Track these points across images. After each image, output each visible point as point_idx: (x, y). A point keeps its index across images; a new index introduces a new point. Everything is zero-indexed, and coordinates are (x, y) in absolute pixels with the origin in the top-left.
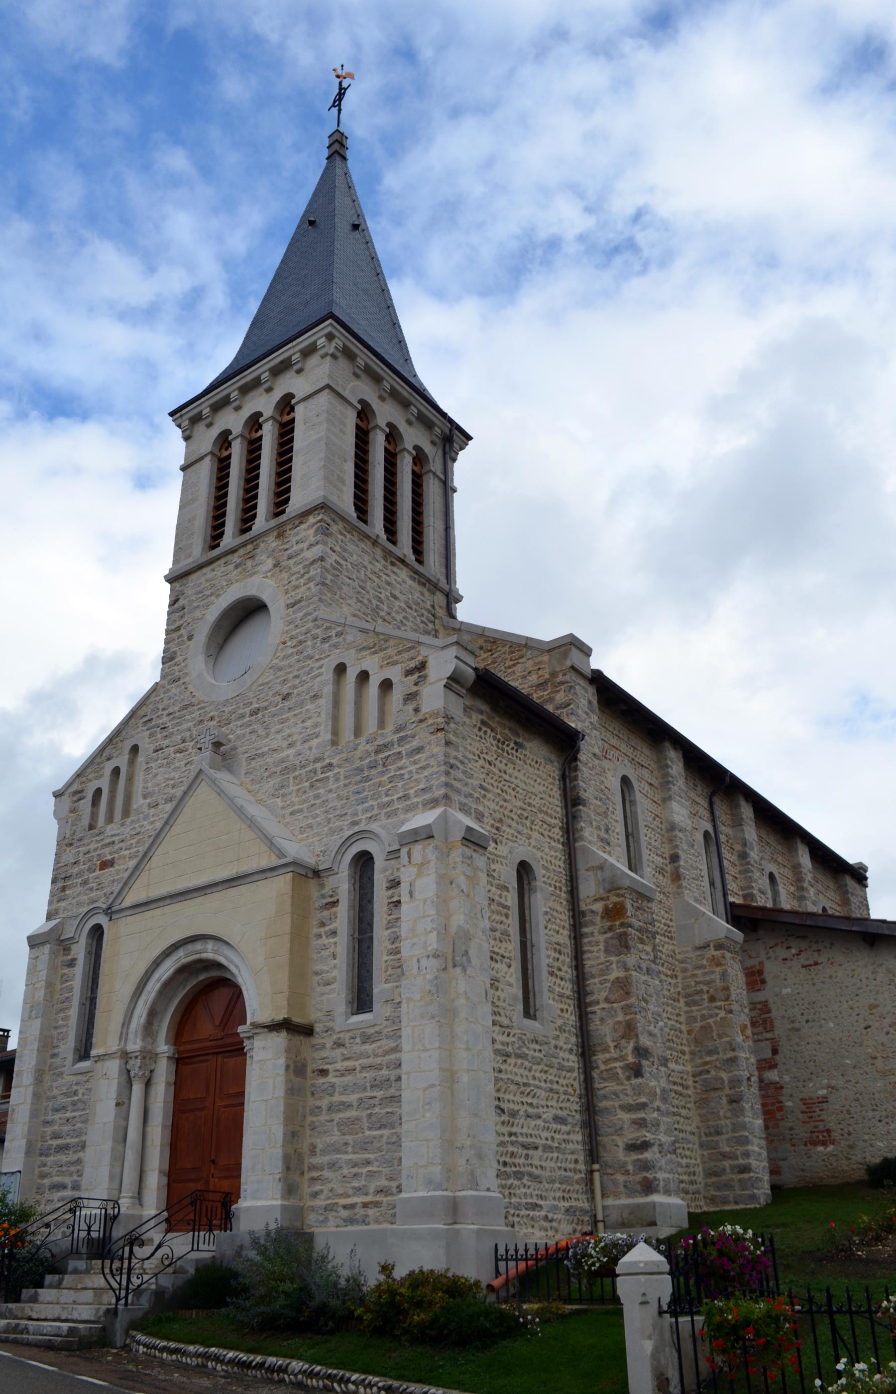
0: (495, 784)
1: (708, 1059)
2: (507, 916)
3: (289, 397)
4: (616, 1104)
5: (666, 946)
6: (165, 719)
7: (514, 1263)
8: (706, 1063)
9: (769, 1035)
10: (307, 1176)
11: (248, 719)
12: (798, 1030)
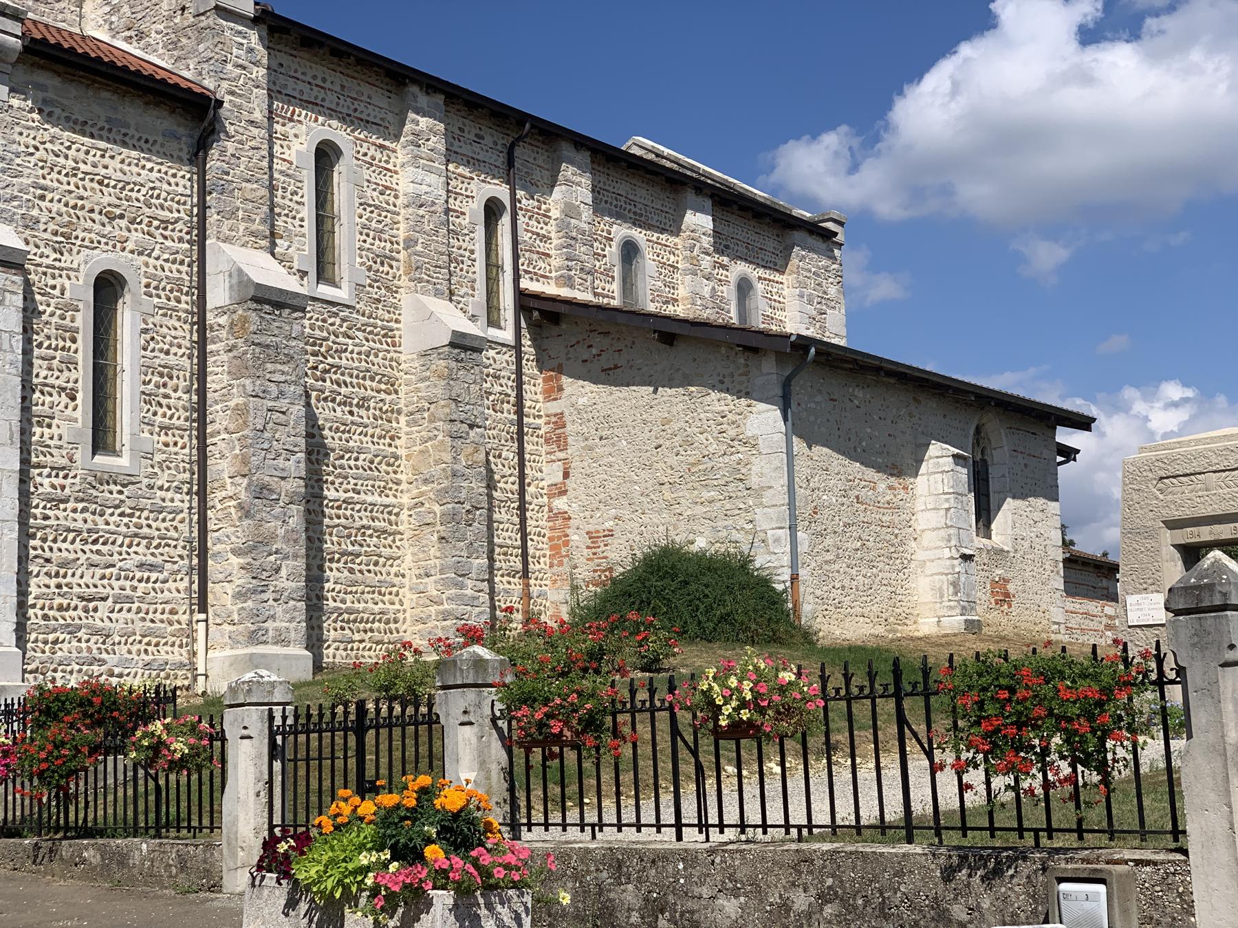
1: (424, 488)
2: (74, 341)
4: (228, 548)
5: (381, 355)
8: (422, 494)
9: (561, 455)
12: (591, 449)
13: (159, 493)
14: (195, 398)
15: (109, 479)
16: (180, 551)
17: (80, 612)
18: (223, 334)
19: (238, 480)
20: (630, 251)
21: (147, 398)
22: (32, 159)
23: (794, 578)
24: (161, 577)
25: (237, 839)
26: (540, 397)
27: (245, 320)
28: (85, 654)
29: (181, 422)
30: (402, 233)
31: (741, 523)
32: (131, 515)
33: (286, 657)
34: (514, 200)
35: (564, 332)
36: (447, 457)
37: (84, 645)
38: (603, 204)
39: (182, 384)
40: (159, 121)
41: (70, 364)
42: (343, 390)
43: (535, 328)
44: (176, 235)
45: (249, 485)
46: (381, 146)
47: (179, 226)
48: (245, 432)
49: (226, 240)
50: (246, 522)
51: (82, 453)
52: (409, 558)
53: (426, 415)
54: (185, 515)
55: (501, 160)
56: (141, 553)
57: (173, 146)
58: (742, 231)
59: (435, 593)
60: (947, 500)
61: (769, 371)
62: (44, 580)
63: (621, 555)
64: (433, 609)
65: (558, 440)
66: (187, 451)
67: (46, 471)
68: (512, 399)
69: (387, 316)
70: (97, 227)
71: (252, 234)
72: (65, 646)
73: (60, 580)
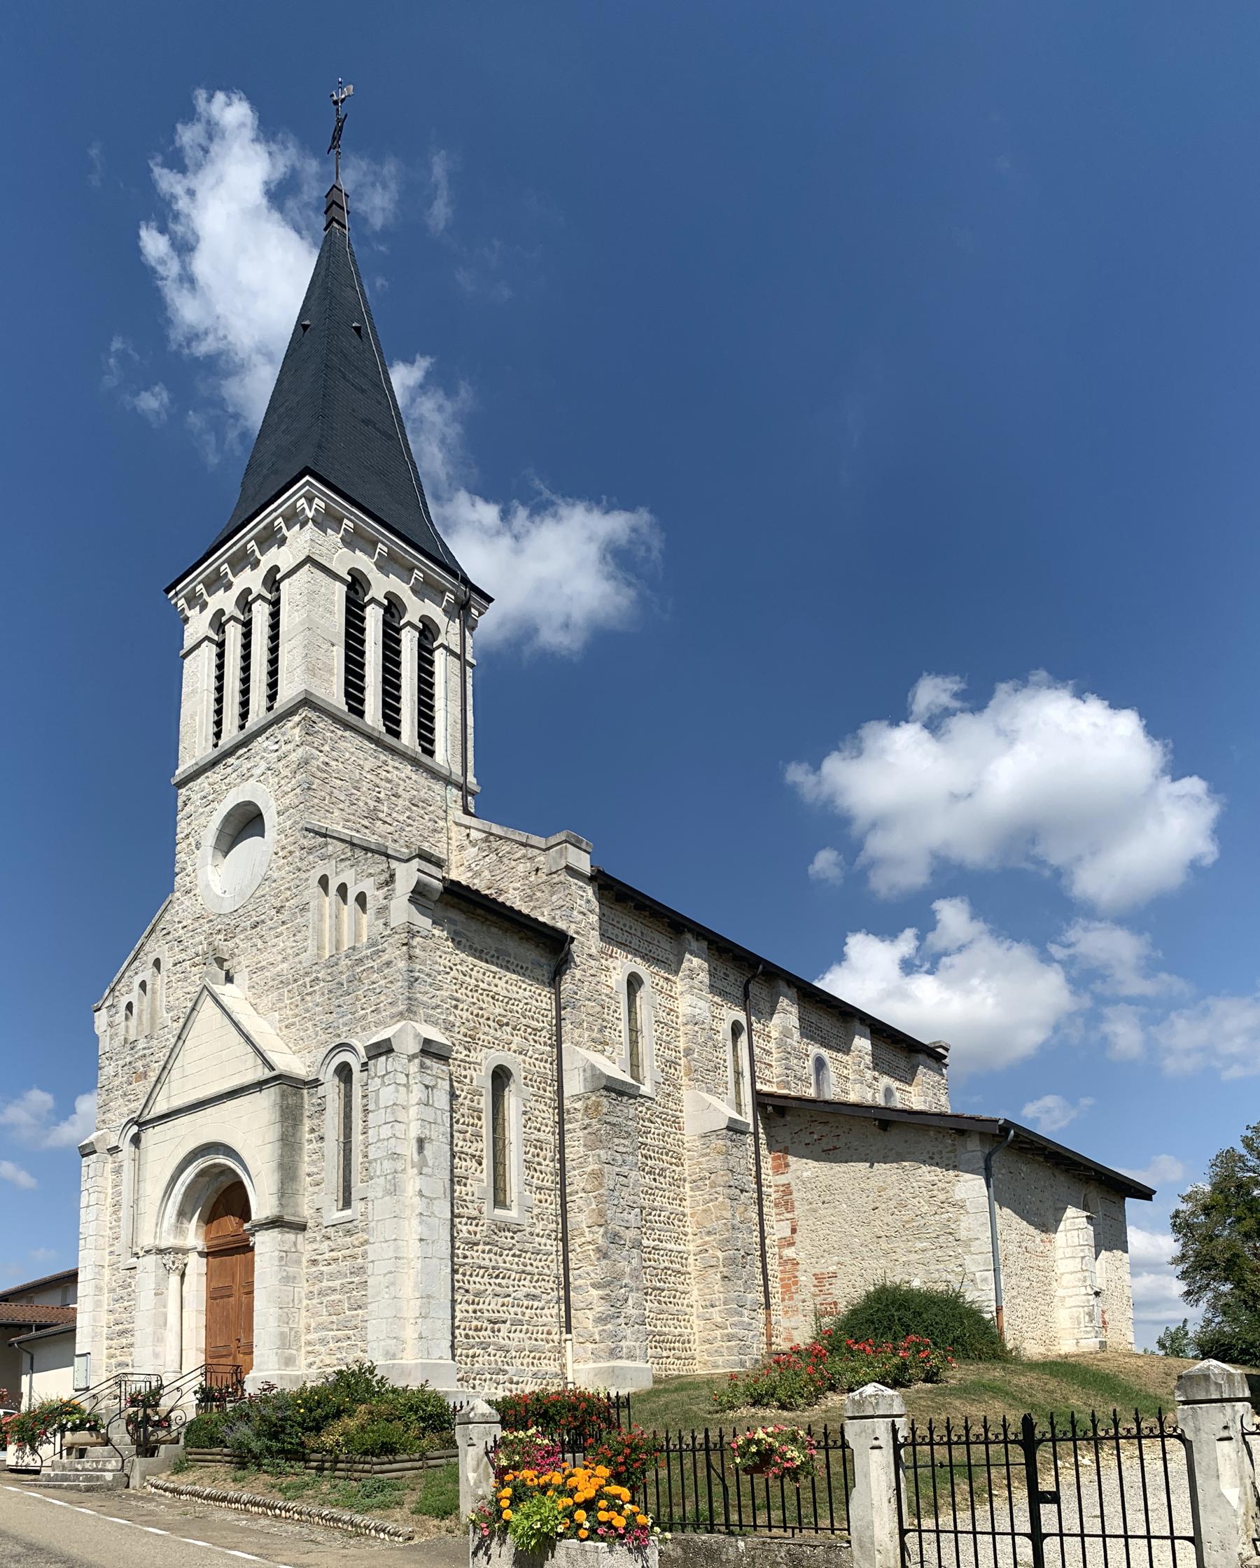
1: (707, 1239)
2: (479, 1119)
3: (275, 569)
6: (181, 932)
7: (983, 1447)
8: (706, 1243)
10: (303, 1350)
12: (815, 1211)
13: (537, 1239)
14: (558, 1166)
15: (504, 1227)
16: (551, 1285)
17: (489, 1332)
18: (579, 1116)
19: (595, 1229)
20: (820, 1064)
21: (528, 1165)
22: (449, 977)
23: (999, 1309)
24: (540, 1305)
25: (873, 1543)
26: (770, 1172)
27: (599, 1104)
28: (493, 1366)
29: (549, 1184)
30: (682, 1045)
31: (951, 1266)
32: (520, 1256)
33: (636, 1369)
34: (750, 1024)
35: (788, 1121)
36: (728, 1214)
37: (492, 1358)
38: (808, 1031)
39: (549, 1155)
40: (529, 953)
41: (477, 1136)
42: (649, 1162)
43: (767, 1120)
44: (542, 1040)
45: (606, 1233)
46: (667, 979)
47: (544, 1033)
48: (601, 1191)
49: (577, 1044)
50: (604, 1262)
51: (487, 1207)
52: (695, 1293)
53: (707, 1182)
54: (553, 1256)
55: (740, 993)
56: (527, 1287)
57: (538, 972)
58: (888, 1055)
59: (720, 1320)
60: (1083, 1251)
61: (974, 1149)
62: (464, 1306)
63: (849, 1290)
64: (718, 1333)
65: (786, 1203)
66: (553, 1206)
67: (464, 1220)
68: (753, 1173)
69: (674, 1107)
70: (492, 1031)
71: (593, 1040)
72: (480, 1359)
73: (475, 1306)
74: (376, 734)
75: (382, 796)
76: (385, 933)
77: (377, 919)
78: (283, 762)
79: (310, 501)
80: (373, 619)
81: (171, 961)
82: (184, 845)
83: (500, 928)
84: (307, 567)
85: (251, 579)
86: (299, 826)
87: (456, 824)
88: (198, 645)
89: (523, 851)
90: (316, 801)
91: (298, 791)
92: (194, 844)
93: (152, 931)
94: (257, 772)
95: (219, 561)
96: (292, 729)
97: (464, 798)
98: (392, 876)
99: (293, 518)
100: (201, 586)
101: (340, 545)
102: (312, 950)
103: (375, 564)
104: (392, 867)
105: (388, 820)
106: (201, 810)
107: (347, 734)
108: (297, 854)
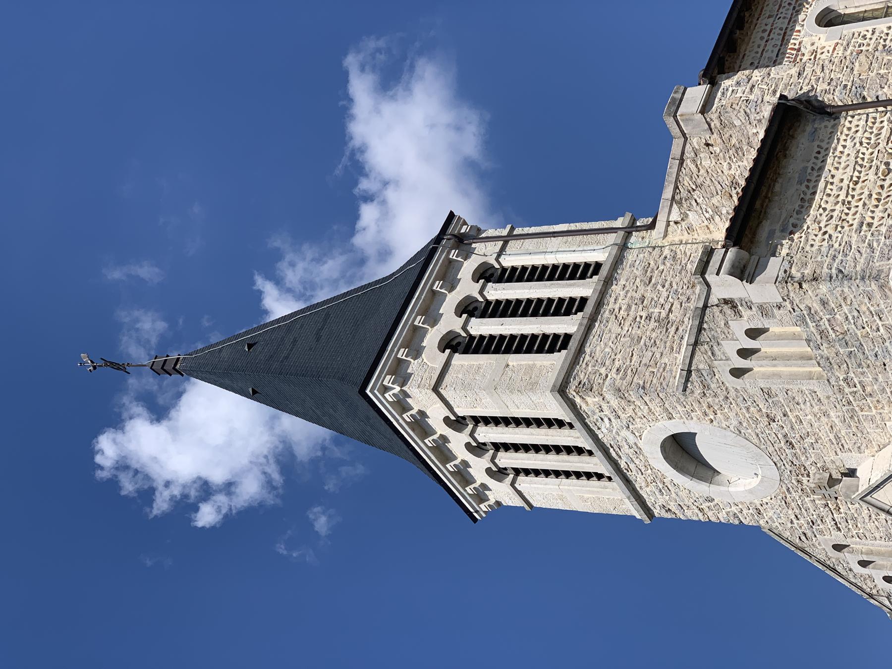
0: (853, 210)
6: (802, 521)
11: (798, 451)
40: (801, 146)
57: (823, 133)
74: (585, 321)
75: (644, 314)
76: (789, 307)
77: (774, 316)
78: (620, 413)
79: (386, 389)
80: (481, 327)
81: (835, 533)
82: (710, 514)
83: (775, 181)
84: (442, 391)
85: (458, 442)
86: (682, 399)
87: (665, 236)
88: (520, 493)
89: (688, 162)
90: (655, 381)
91: (647, 399)
92: (708, 504)
93: (803, 550)
94: (631, 439)
95: (445, 472)
96: (588, 404)
97: (639, 229)
98: (726, 302)
99: (402, 405)
100: (467, 489)
101: (420, 360)
102: (814, 385)
103: (432, 327)
104: (716, 302)
105: (667, 307)
106: (674, 495)
107: (588, 350)
108: (710, 400)
